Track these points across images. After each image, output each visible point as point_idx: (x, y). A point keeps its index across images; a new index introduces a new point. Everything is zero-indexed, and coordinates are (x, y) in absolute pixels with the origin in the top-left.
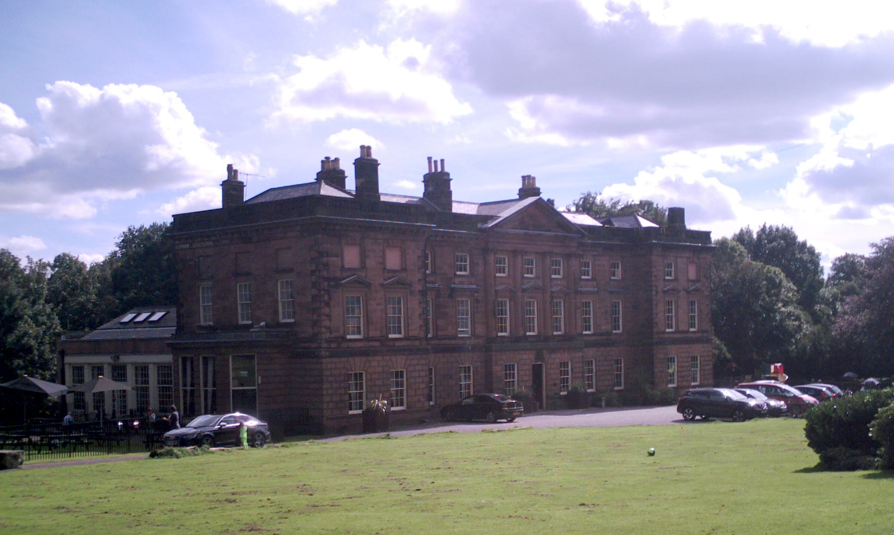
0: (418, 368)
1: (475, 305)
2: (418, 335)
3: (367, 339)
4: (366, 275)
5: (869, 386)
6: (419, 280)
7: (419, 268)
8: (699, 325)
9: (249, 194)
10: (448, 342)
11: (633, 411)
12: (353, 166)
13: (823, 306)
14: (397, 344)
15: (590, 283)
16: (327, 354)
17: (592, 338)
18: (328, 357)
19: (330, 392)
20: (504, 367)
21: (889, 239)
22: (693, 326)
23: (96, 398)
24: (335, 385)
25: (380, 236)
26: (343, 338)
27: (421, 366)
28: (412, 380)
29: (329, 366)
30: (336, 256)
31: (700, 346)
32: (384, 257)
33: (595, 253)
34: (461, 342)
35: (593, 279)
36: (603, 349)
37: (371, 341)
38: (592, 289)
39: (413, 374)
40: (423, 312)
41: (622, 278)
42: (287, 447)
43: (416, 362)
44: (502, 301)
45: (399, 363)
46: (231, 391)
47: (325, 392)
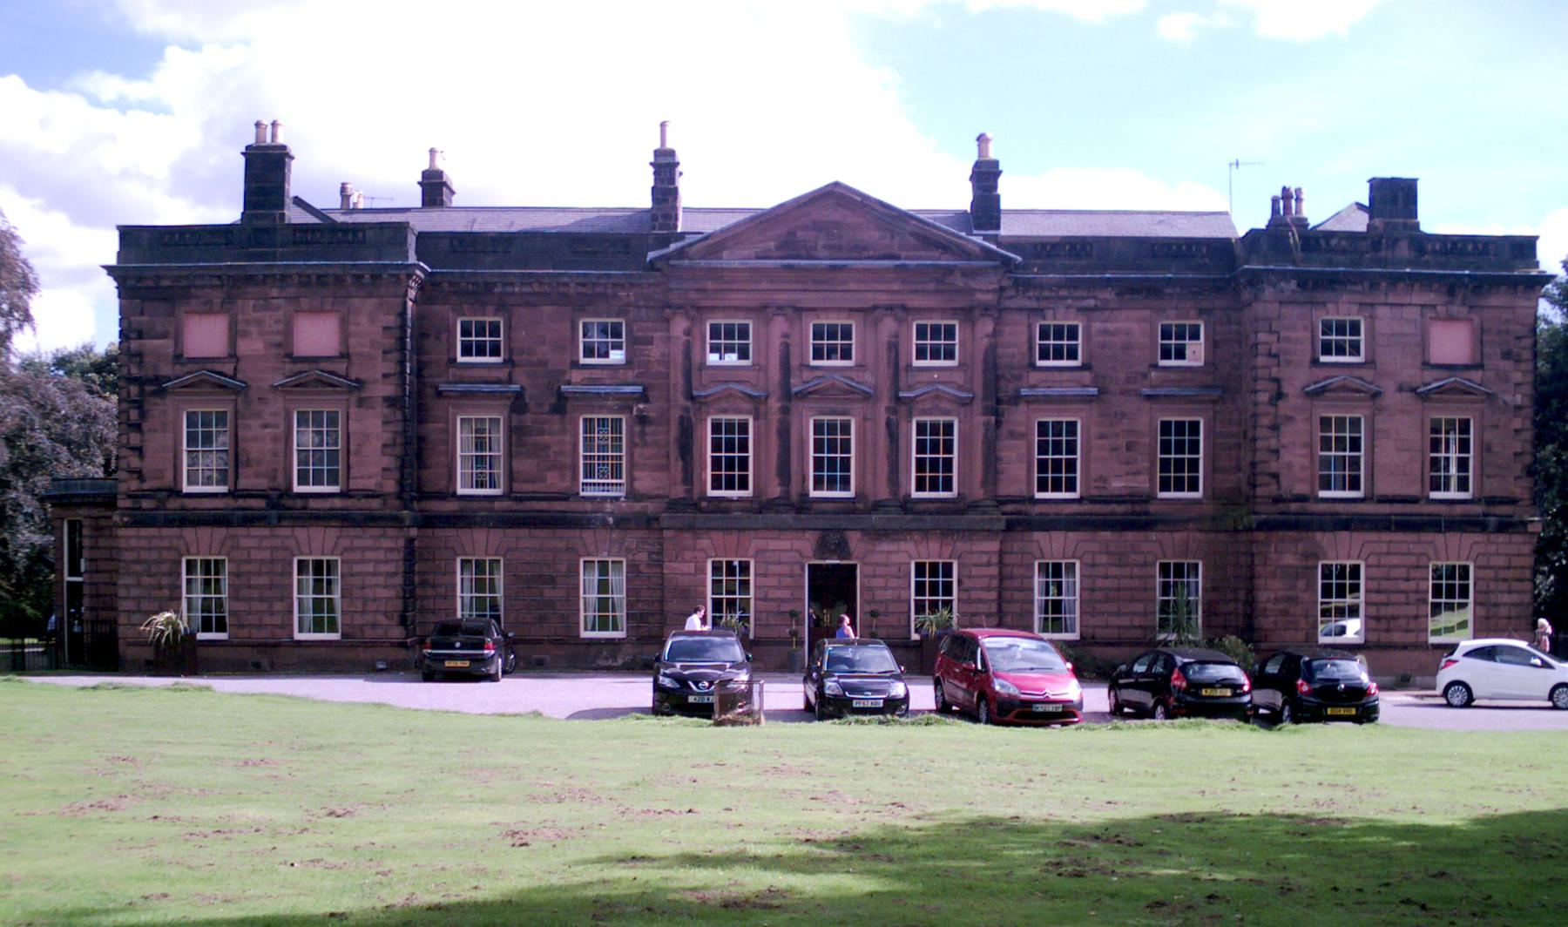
2: (378, 489)
4: (235, 369)
7: (385, 352)
8: (1480, 485)
9: (1366, 202)
10: (544, 505)
14: (313, 504)
15: (1078, 374)
16: (126, 519)
17: (1075, 508)
18: (126, 525)
19: (134, 592)
22: (1177, 474)
23: (765, 615)
24: (146, 580)
25: (275, 292)
26: (175, 492)
27: (382, 552)
28: (357, 581)
29: (133, 543)
30: (164, 336)
32: (288, 332)
33: (1092, 303)
34: (588, 506)
35: (1085, 367)
36: (1107, 535)
37: (245, 497)
38: (1078, 391)
39: (358, 568)
40: (395, 439)
41: (1206, 363)
42: (863, 723)
43: (368, 543)
44: (1060, 423)
45: (318, 543)
46: (65, 585)
47: (122, 592)
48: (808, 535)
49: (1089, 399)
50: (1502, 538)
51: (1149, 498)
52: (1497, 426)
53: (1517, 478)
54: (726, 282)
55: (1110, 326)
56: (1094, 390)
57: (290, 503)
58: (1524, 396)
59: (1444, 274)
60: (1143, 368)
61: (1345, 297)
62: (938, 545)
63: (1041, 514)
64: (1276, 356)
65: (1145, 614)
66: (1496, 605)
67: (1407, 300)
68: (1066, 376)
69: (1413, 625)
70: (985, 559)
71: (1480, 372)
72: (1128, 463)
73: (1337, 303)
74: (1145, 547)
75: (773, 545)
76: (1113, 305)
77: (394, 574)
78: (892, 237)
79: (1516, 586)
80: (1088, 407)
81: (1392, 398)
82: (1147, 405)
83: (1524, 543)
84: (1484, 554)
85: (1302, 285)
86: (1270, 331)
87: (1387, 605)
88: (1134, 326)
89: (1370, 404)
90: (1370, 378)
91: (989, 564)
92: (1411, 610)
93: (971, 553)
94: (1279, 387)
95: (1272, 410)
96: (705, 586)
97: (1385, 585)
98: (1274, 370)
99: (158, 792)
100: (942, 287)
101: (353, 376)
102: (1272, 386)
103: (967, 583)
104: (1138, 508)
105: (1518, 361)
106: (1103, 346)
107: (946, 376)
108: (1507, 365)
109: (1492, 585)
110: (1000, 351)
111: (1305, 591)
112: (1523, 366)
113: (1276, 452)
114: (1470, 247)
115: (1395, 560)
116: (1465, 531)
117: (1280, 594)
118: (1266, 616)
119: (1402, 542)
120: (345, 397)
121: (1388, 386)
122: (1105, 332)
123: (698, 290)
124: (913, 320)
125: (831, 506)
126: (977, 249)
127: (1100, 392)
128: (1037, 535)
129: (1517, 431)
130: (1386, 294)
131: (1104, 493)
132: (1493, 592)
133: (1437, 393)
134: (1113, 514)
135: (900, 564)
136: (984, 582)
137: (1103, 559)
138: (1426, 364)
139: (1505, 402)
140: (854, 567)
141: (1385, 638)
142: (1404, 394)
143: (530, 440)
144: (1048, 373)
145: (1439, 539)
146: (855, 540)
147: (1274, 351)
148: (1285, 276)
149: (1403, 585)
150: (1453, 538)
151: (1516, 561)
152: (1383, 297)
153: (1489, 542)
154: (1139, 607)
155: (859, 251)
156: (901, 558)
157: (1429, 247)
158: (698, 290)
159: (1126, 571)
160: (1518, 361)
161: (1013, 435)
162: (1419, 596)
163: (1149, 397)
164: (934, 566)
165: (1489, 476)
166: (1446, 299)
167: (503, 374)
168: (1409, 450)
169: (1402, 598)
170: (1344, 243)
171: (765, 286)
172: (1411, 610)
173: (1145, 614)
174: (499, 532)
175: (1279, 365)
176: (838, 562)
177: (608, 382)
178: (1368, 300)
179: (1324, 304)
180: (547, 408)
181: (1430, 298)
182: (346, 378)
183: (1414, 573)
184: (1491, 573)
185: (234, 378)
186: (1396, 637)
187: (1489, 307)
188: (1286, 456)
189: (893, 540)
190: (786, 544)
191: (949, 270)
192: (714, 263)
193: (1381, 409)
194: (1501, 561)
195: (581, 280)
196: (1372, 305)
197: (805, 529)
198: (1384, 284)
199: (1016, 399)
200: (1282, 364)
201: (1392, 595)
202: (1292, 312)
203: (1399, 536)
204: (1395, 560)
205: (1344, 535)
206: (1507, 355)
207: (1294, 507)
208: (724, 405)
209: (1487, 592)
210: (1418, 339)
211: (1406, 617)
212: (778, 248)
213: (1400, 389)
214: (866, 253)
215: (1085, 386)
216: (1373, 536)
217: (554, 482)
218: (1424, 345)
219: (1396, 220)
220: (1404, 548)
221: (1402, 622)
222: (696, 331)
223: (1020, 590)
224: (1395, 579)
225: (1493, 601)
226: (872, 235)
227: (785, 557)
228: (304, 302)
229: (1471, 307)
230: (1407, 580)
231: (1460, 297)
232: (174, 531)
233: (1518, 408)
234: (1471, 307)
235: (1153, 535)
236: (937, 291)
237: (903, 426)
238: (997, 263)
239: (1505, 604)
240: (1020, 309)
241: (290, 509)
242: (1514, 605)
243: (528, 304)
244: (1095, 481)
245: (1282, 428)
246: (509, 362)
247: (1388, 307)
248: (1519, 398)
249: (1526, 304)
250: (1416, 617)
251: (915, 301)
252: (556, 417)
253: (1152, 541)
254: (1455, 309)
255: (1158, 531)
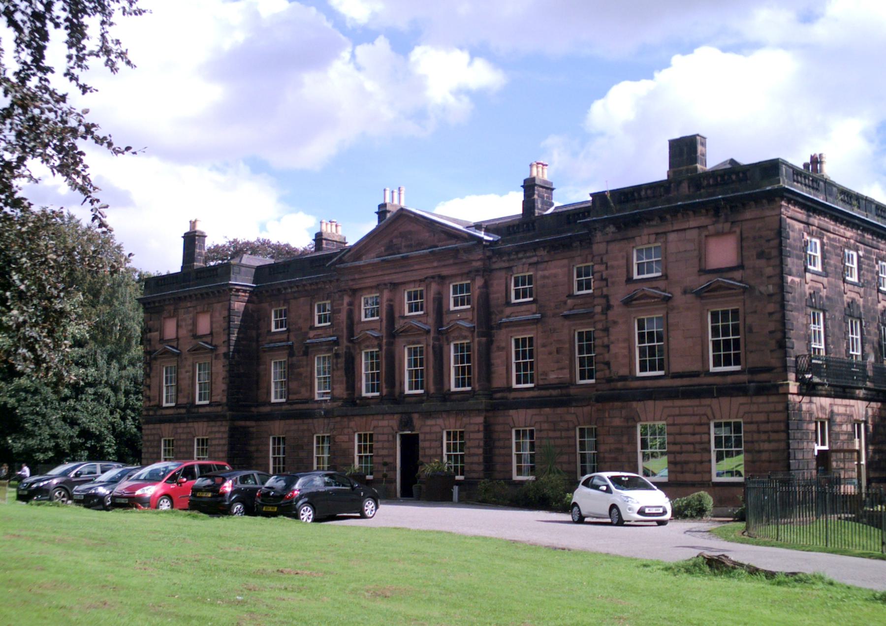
0: (217, 435)
1: (335, 361)
3: (177, 406)
5: (844, 502)
6: (224, 342)
11: (390, 506)
12: (182, 240)
13: (238, 306)
15: (529, 306)
20: (374, 439)
21: (468, 93)
31: (742, 400)
33: (535, 259)
34: (316, 406)
36: (547, 410)
38: (530, 317)
48: (396, 416)
49: (536, 321)
50: (761, 399)
51: (571, 383)
52: (755, 312)
53: (772, 351)
54: (364, 273)
55: (546, 273)
56: (538, 315)
57: (196, 410)
58: (774, 285)
59: (708, 201)
60: (564, 298)
61: (646, 231)
62: (454, 421)
63: (514, 399)
64: (606, 280)
65: (569, 463)
66: (760, 452)
67: (686, 226)
68: (524, 308)
69: (699, 468)
70: (477, 428)
71: (741, 271)
72: (558, 362)
73: (640, 236)
74: (569, 417)
75: (381, 423)
76: (546, 259)
77: (224, 445)
78: (434, 235)
79: (774, 436)
80: (535, 326)
81: (680, 299)
82: (567, 323)
83: (779, 402)
84: (749, 413)
85: (619, 228)
86: (602, 262)
87: (681, 453)
88: (559, 271)
89: (665, 305)
90: (663, 287)
91: (479, 431)
92: (697, 457)
93: (470, 424)
94: (608, 301)
95: (603, 317)
96: (354, 449)
97: (679, 438)
98: (605, 290)
99: (606, 610)
100: (457, 261)
101: (214, 343)
102: (603, 301)
103: (438, 444)
104: (564, 392)
105: (769, 259)
106: (543, 286)
107: (464, 315)
108: (762, 263)
109: (756, 437)
110: (492, 296)
111: (628, 443)
112: (773, 262)
113: (608, 346)
114: (734, 177)
115: (685, 420)
116: (731, 396)
117: (613, 446)
118: (605, 462)
119: (689, 406)
120: (210, 355)
121: (677, 291)
122: (544, 277)
123: (352, 280)
124: (450, 283)
125: (414, 399)
126: (466, 236)
127: (542, 316)
128: (512, 412)
129: (770, 314)
130: (672, 224)
131: (546, 382)
132: (757, 441)
133: (706, 292)
134: (550, 396)
135: (436, 433)
136: (476, 443)
137: (545, 426)
138: (703, 271)
139: (760, 292)
140: (417, 435)
141: (681, 477)
142: (688, 296)
143: (296, 371)
144: (515, 307)
145: (714, 402)
146: (416, 419)
147: (604, 277)
148: (605, 223)
149: (691, 438)
150: (725, 401)
151: (773, 417)
152: (670, 225)
153: (752, 403)
154: (565, 458)
155: (420, 245)
156: (437, 429)
157: (705, 183)
158: (352, 280)
159: (558, 434)
160: (769, 259)
161: (500, 349)
162: (702, 446)
163: (566, 317)
164: (455, 433)
165: (751, 352)
166: (714, 219)
167: (285, 336)
168: (692, 337)
169: (690, 448)
170: (649, 192)
171: (380, 273)
172: (697, 457)
173: (569, 463)
174: (282, 422)
175: (607, 286)
176: (409, 432)
177: (324, 335)
178: (660, 231)
179: (634, 238)
180: (301, 353)
181: (702, 220)
182: (211, 345)
183: (698, 429)
184: (754, 427)
185: (177, 349)
186: (688, 477)
187: (746, 220)
188: (614, 349)
189: (434, 418)
190: (385, 423)
191: (457, 250)
192: (357, 263)
193: (673, 309)
194: (762, 417)
195: (310, 282)
196: (665, 233)
197: (393, 414)
198: (668, 217)
199: (500, 326)
200: (609, 284)
201: (556, 440)
202: (615, 247)
203: (687, 402)
204: (685, 420)
205: (650, 403)
206: (761, 255)
207: (620, 384)
208: (367, 343)
209: (752, 442)
210: (696, 253)
211: (695, 462)
212: (386, 250)
213: (685, 292)
214: (423, 247)
215: (534, 313)
216: (669, 403)
217: (304, 393)
218: (701, 256)
219: (681, 168)
220: (690, 410)
221: (692, 466)
222: (356, 302)
223: (504, 448)
224: (687, 434)
225: (757, 449)
226: (425, 235)
227: (386, 430)
228: (199, 309)
229: (733, 223)
230: (694, 434)
231: (723, 217)
232: (157, 426)
233: (770, 295)
234: (733, 223)
235: (572, 410)
236: (455, 264)
237: (445, 348)
238: (475, 242)
239: (766, 451)
240: (500, 269)
241: (194, 413)
242: (773, 451)
243: (295, 298)
244: (541, 375)
245: (611, 329)
246: (288, 330)
247: (676, 233)
248: (771, 287)
249: (774, 213)
250: (701, 462)
251: (445, 272)
252: (305, 357)
253: (571, 413)
254: (720, 226)
255: (574, 407)
